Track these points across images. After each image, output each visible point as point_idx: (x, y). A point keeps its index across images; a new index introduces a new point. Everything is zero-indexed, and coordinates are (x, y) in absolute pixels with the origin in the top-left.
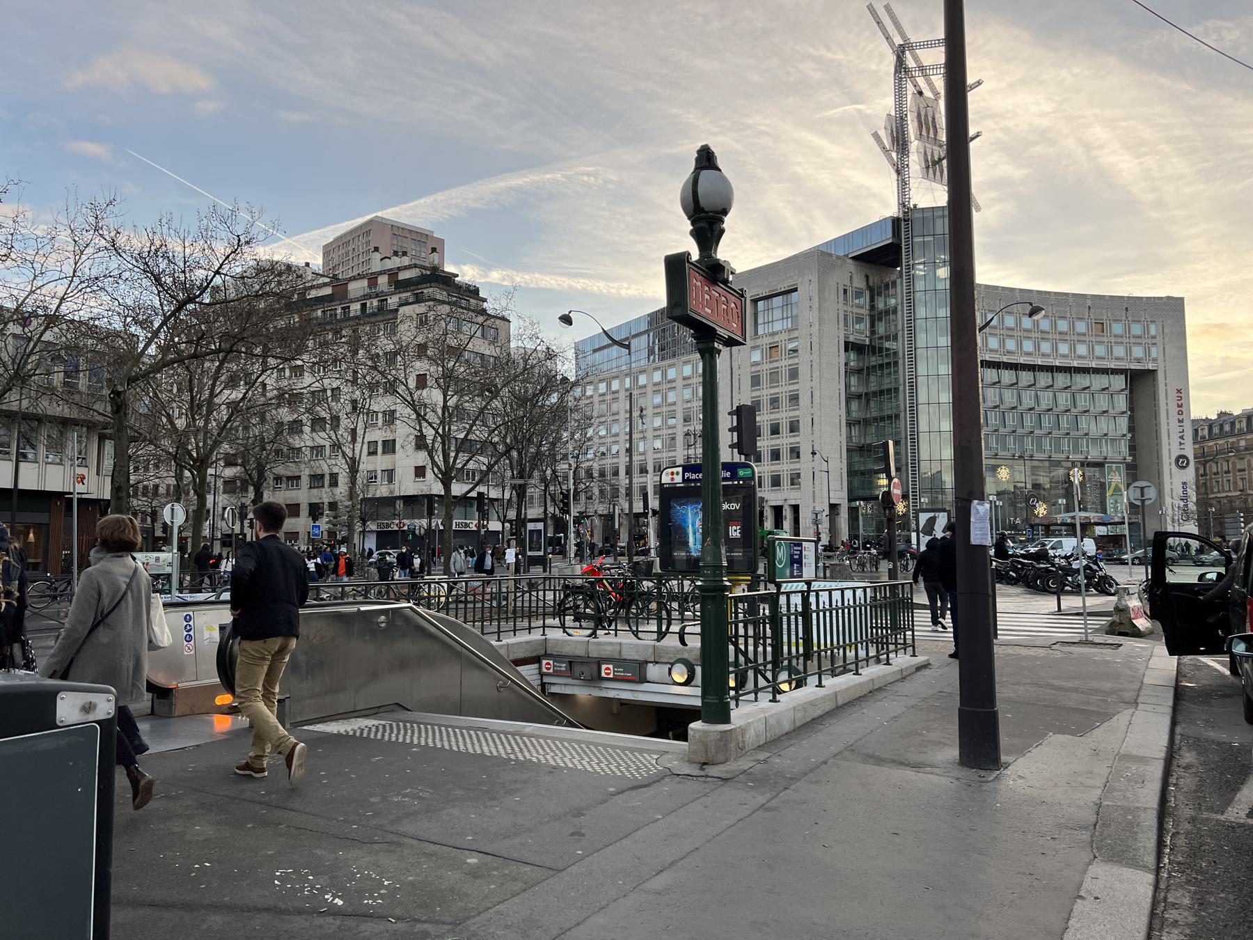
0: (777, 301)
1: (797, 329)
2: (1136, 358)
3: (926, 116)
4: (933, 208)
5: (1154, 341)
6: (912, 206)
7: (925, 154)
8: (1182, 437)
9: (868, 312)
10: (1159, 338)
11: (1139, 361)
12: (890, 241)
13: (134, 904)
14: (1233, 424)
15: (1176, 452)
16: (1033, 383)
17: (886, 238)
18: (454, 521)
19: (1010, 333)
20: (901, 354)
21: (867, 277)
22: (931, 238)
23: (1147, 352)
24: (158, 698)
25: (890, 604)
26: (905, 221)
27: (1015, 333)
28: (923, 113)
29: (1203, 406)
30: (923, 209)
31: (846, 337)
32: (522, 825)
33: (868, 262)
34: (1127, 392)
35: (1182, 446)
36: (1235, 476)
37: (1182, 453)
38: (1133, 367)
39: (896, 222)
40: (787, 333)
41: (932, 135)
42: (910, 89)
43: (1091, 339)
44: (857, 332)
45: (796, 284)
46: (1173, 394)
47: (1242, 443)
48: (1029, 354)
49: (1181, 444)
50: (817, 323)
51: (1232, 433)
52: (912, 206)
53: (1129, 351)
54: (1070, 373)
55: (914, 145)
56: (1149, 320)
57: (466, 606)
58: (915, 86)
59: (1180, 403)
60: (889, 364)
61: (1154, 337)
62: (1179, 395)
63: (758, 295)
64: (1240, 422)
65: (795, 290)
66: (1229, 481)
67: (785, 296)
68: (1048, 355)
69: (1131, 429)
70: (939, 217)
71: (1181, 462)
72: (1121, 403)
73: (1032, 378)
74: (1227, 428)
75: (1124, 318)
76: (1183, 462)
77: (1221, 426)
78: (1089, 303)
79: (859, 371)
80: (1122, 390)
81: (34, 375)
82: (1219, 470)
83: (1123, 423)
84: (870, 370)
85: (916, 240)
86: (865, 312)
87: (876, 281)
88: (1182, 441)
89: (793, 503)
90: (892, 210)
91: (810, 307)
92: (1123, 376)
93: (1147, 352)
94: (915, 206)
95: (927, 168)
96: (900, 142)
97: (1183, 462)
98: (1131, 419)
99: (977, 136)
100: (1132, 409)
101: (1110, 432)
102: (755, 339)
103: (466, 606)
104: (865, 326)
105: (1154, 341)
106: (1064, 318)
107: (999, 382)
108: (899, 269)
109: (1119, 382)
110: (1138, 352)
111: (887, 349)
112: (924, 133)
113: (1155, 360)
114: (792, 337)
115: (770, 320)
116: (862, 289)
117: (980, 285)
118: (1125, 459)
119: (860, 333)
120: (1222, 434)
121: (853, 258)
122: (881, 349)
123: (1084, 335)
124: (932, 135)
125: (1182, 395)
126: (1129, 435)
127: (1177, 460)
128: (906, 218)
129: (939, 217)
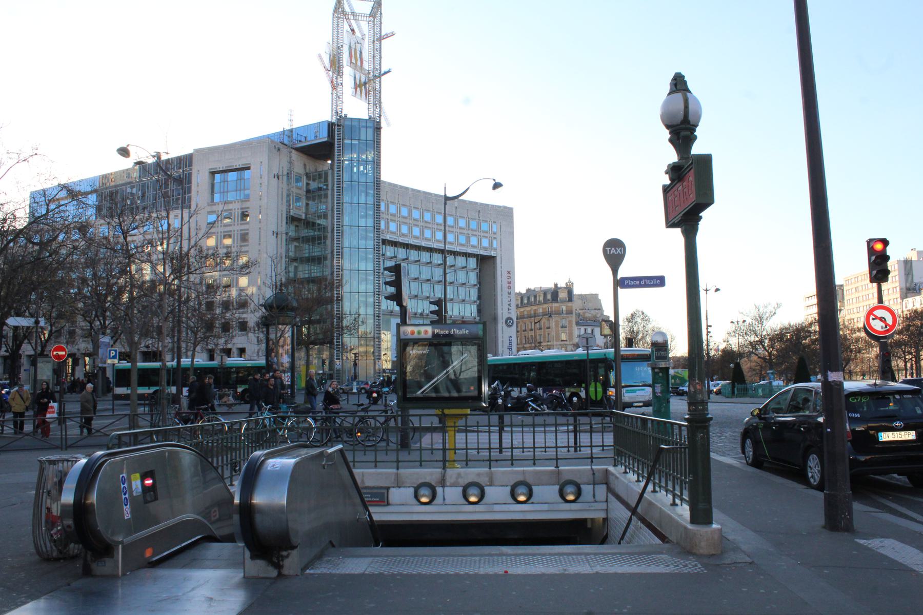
0: (232, 176)
1: (249, 201)
2: (481, 246)
3: (355, 49)
4: (359, 119)
5: (495, 236)
6: (343, 116)
7: (355, 78)
8: (509, 305)
10: (498, 233)
11: (485, 249)
12: (326, 140)
14: (535, 297)
15: (506, 316)
17: (323, 137)
19: (393, 218)
20: (329, 230)
21: (305, 165)
22: (356, 142)
23: (491, 243)
24: (252, 558)
25: (252, 434)
26: (338, 125)
27: (407, 221)
28: (353, 46)
29: (521, 287)
30: (352, 119)
31: (288, 212)
34: (477, 271)
35: (510, 311)
36: (544, 332)
37: (510, 316)
38: (482, 253)
39: (331, 126)
40: (240, 203)
41: (359, 63)
42: (346, 27)
43: (491, 235)
44: (296, 208)
45: (250, 164)
46: (505, 275)
47: (541, 311)
48: (416, 238)
49: (509, 309)
50: (266, 198)
51: (535, 304)
52: (343, 116)
53: (480, 241)
54: (466, 257)
55: (348, 71)
56: (492, 221)
57: (534, 450)
58: (350, 26)
59: (509, 280)
60: (319, 238)
61: (495, 233)
62: (509, 275)
63: (216, 168)
64: (540, 296)
65: (248, 168)
66: (540, 335)
67: (239, 172)
68: (463, 245)
69: (479, 297)
70: (363, 127)
71: (509, 322)
72: (473, 278)
74: (532, 299)
75: (477, 218)
76: (510, 322)
77: (529, 298)
79: (296, 239)
80: (475, 269)
82: (533, 327)
83: (474, 293)
84: (307, 240)
85: (346, 141)
87: (311, 169)
88: (510, 308)
89: (241, 346)
90: (326, 115)
91: (261, 184)
92: (475, 259)
93: (491, 243)
94: (346, 116)
95: (356, 89)
96: (335, 65)
97: (510, 322)
98: (479, 290)
99: (389, 71)
100: (480, 283)
101: (467, 299)
102: (211, 205)
103: (534, 450)
105: (495, 236)
106: (486, 221)
107: (431, 262)
108: (329, 162)
109: (473, 263)
110: (485, 243)
111: (319, 225)
112: (353, 61)
113: (495, 249)
114: (244, 207)
115: (226, 190)
116: (301, 174)
117: (385, 182)
118: (475, 319)
120: (529, 304)
122: (314, 224)
123: (487, 232)
124: (359, 63)
125: (511, 275)
126: (478, 302)
127: (506, 321)
129: (363, 127)
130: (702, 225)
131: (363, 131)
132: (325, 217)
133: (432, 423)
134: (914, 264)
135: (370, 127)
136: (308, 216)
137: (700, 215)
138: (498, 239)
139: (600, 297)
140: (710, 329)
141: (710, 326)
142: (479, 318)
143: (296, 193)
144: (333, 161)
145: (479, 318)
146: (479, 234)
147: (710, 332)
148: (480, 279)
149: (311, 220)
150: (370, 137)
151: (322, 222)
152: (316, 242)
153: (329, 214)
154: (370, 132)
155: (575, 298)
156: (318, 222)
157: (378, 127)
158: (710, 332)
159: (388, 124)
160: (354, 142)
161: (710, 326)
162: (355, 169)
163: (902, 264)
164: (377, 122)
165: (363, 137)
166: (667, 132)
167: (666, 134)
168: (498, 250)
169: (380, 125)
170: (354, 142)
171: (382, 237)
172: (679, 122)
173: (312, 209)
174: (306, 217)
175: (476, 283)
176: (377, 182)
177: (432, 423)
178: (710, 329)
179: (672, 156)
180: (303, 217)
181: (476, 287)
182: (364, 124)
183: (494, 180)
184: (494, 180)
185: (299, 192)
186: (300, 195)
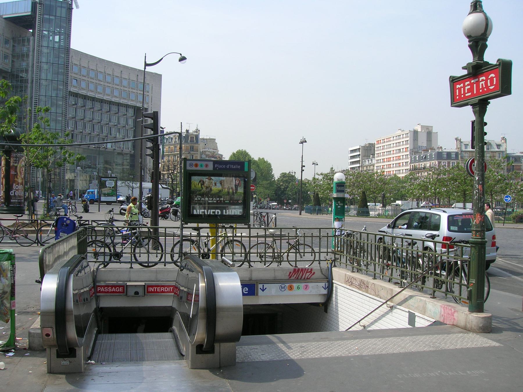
9: (11, 53)
12: (30, 14)
13: (492, 266)
16: (117, 112)
18: (192, 206)
20: (30, 81)
22: (53, 18)
26: (40, 4)
32: (147, 366)
33: (14, 23)
70: (59, 7)
73: (117, 110)
78: (122, 69)
80: (132, 117)
81: (492, 198)
86: (10, 52)
104: (9, 61)
109: (131, 112)
111: (21, 77)
118: (131, 152)
119: (6, 64)
121: (6, 19)
122: (17, 76)
128: (41, 3)
129: (59, 7)
130: (489, 107)
131: (59, 9)
132: (27, 71)
133: (258, 233)
134: (419, 134)
135: (64, 7)
136: (13, 70)
137: (489, 101)
138: (150, 96)
139: (216, 141)
140: (304, 168)
141: (304, 166)
142: (133, 151)
143: (5, 52)
144: (34, 29)
145: (133, 151)
146: (137, 91)
147: (303, 170)
148: (135, 124)
149: (15, 73)
150: (64, 15)
151: (24, 75)
152: (19, 90)
153: (30, 69)
154: (64, 11)
155: (199, 140)
156: (21, 75)
157: (71, 8)
158: (303, 170)
159: (77, 7)
160: (51, 17)
161: (304, 166)
162: (51, 38)
163: (412, 134)
164: (70, 4)
165: (58, 14)
166: (467, 40)
167: (466, 42)
168: (150, 104)
169: (72, 6)
170: (51, 17)
171: (68, 90)
172: (480, 34)
173: (17, 65)
174: (12, 71)
175: (132, 127)
176: (67, 49)
177: (258, 233)
178: (304, 168)
179: (469, 58)
180: (10, 71)
181: (133, 129)
182: (60, 5)
183: (181, 54)
184: (181, 54)
185: (7, 51)
186: (8, 53)
